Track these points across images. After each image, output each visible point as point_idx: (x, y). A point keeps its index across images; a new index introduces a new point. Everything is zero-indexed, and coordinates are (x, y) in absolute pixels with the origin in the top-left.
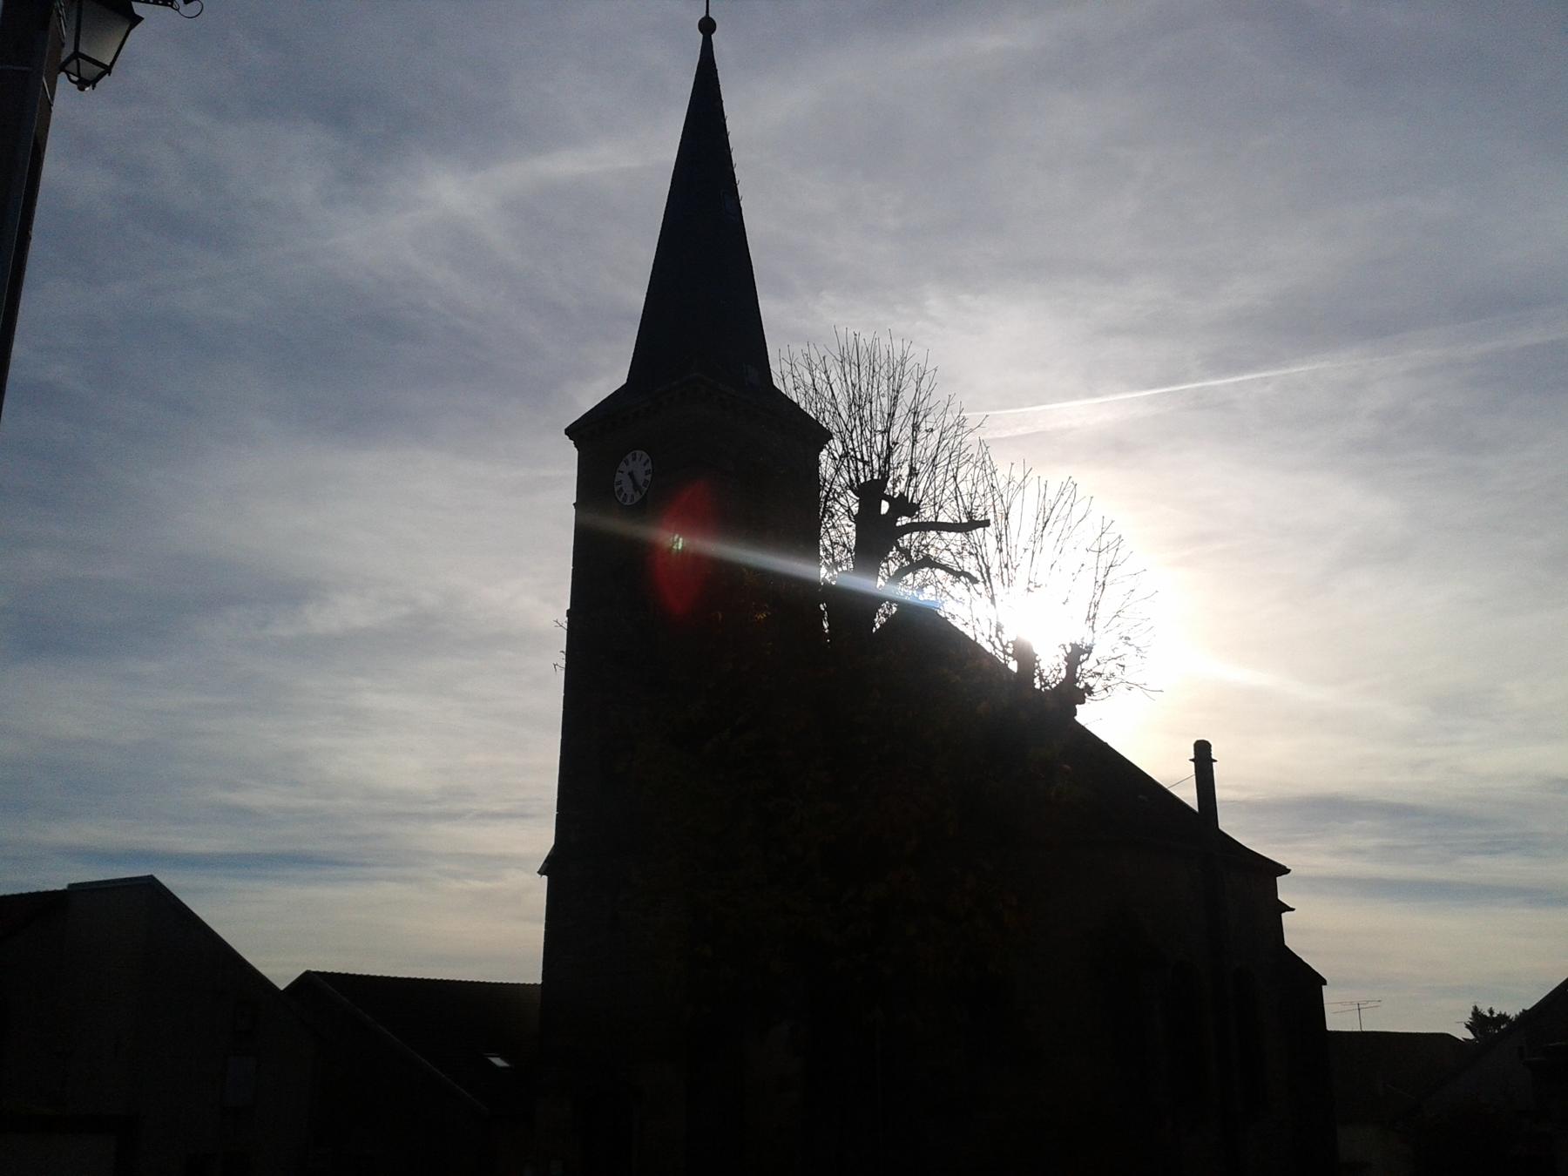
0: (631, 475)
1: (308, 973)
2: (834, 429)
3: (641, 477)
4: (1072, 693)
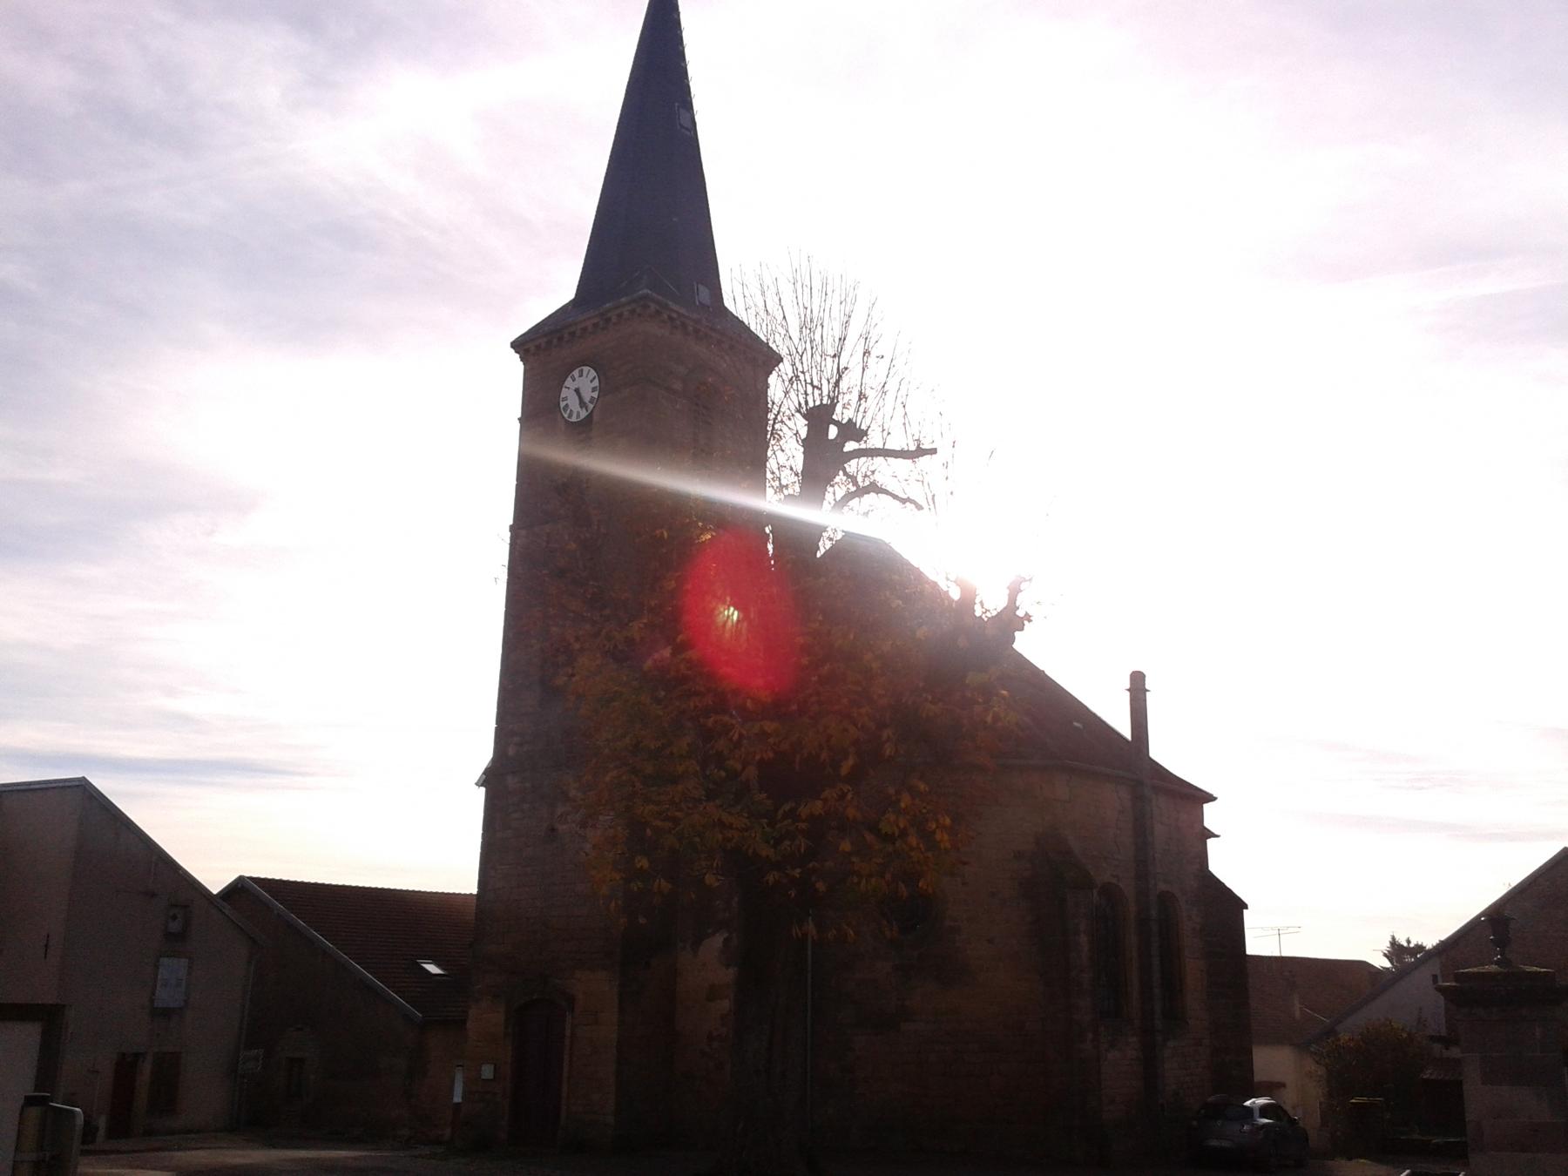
0: (577, 391)
1: (241, 879)
2: (783, 352)
3: (588, 395)
4: (1011, 621)
